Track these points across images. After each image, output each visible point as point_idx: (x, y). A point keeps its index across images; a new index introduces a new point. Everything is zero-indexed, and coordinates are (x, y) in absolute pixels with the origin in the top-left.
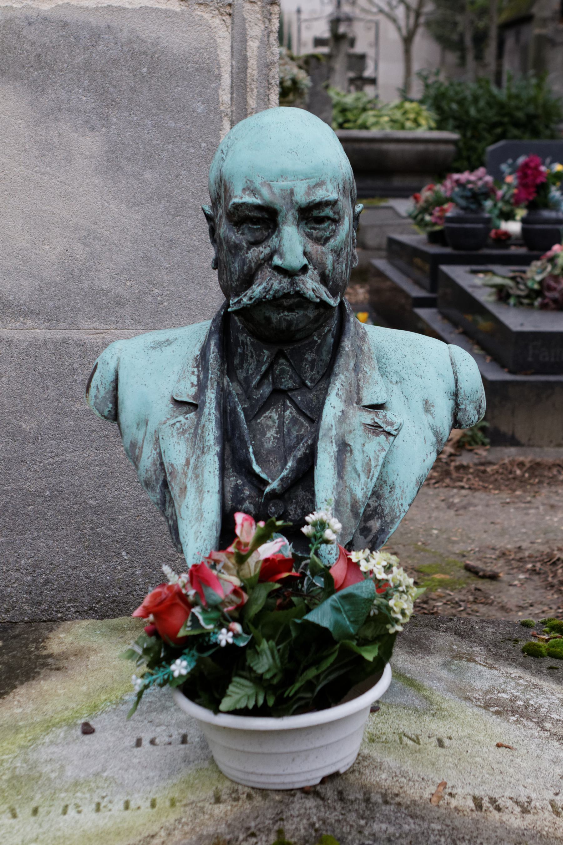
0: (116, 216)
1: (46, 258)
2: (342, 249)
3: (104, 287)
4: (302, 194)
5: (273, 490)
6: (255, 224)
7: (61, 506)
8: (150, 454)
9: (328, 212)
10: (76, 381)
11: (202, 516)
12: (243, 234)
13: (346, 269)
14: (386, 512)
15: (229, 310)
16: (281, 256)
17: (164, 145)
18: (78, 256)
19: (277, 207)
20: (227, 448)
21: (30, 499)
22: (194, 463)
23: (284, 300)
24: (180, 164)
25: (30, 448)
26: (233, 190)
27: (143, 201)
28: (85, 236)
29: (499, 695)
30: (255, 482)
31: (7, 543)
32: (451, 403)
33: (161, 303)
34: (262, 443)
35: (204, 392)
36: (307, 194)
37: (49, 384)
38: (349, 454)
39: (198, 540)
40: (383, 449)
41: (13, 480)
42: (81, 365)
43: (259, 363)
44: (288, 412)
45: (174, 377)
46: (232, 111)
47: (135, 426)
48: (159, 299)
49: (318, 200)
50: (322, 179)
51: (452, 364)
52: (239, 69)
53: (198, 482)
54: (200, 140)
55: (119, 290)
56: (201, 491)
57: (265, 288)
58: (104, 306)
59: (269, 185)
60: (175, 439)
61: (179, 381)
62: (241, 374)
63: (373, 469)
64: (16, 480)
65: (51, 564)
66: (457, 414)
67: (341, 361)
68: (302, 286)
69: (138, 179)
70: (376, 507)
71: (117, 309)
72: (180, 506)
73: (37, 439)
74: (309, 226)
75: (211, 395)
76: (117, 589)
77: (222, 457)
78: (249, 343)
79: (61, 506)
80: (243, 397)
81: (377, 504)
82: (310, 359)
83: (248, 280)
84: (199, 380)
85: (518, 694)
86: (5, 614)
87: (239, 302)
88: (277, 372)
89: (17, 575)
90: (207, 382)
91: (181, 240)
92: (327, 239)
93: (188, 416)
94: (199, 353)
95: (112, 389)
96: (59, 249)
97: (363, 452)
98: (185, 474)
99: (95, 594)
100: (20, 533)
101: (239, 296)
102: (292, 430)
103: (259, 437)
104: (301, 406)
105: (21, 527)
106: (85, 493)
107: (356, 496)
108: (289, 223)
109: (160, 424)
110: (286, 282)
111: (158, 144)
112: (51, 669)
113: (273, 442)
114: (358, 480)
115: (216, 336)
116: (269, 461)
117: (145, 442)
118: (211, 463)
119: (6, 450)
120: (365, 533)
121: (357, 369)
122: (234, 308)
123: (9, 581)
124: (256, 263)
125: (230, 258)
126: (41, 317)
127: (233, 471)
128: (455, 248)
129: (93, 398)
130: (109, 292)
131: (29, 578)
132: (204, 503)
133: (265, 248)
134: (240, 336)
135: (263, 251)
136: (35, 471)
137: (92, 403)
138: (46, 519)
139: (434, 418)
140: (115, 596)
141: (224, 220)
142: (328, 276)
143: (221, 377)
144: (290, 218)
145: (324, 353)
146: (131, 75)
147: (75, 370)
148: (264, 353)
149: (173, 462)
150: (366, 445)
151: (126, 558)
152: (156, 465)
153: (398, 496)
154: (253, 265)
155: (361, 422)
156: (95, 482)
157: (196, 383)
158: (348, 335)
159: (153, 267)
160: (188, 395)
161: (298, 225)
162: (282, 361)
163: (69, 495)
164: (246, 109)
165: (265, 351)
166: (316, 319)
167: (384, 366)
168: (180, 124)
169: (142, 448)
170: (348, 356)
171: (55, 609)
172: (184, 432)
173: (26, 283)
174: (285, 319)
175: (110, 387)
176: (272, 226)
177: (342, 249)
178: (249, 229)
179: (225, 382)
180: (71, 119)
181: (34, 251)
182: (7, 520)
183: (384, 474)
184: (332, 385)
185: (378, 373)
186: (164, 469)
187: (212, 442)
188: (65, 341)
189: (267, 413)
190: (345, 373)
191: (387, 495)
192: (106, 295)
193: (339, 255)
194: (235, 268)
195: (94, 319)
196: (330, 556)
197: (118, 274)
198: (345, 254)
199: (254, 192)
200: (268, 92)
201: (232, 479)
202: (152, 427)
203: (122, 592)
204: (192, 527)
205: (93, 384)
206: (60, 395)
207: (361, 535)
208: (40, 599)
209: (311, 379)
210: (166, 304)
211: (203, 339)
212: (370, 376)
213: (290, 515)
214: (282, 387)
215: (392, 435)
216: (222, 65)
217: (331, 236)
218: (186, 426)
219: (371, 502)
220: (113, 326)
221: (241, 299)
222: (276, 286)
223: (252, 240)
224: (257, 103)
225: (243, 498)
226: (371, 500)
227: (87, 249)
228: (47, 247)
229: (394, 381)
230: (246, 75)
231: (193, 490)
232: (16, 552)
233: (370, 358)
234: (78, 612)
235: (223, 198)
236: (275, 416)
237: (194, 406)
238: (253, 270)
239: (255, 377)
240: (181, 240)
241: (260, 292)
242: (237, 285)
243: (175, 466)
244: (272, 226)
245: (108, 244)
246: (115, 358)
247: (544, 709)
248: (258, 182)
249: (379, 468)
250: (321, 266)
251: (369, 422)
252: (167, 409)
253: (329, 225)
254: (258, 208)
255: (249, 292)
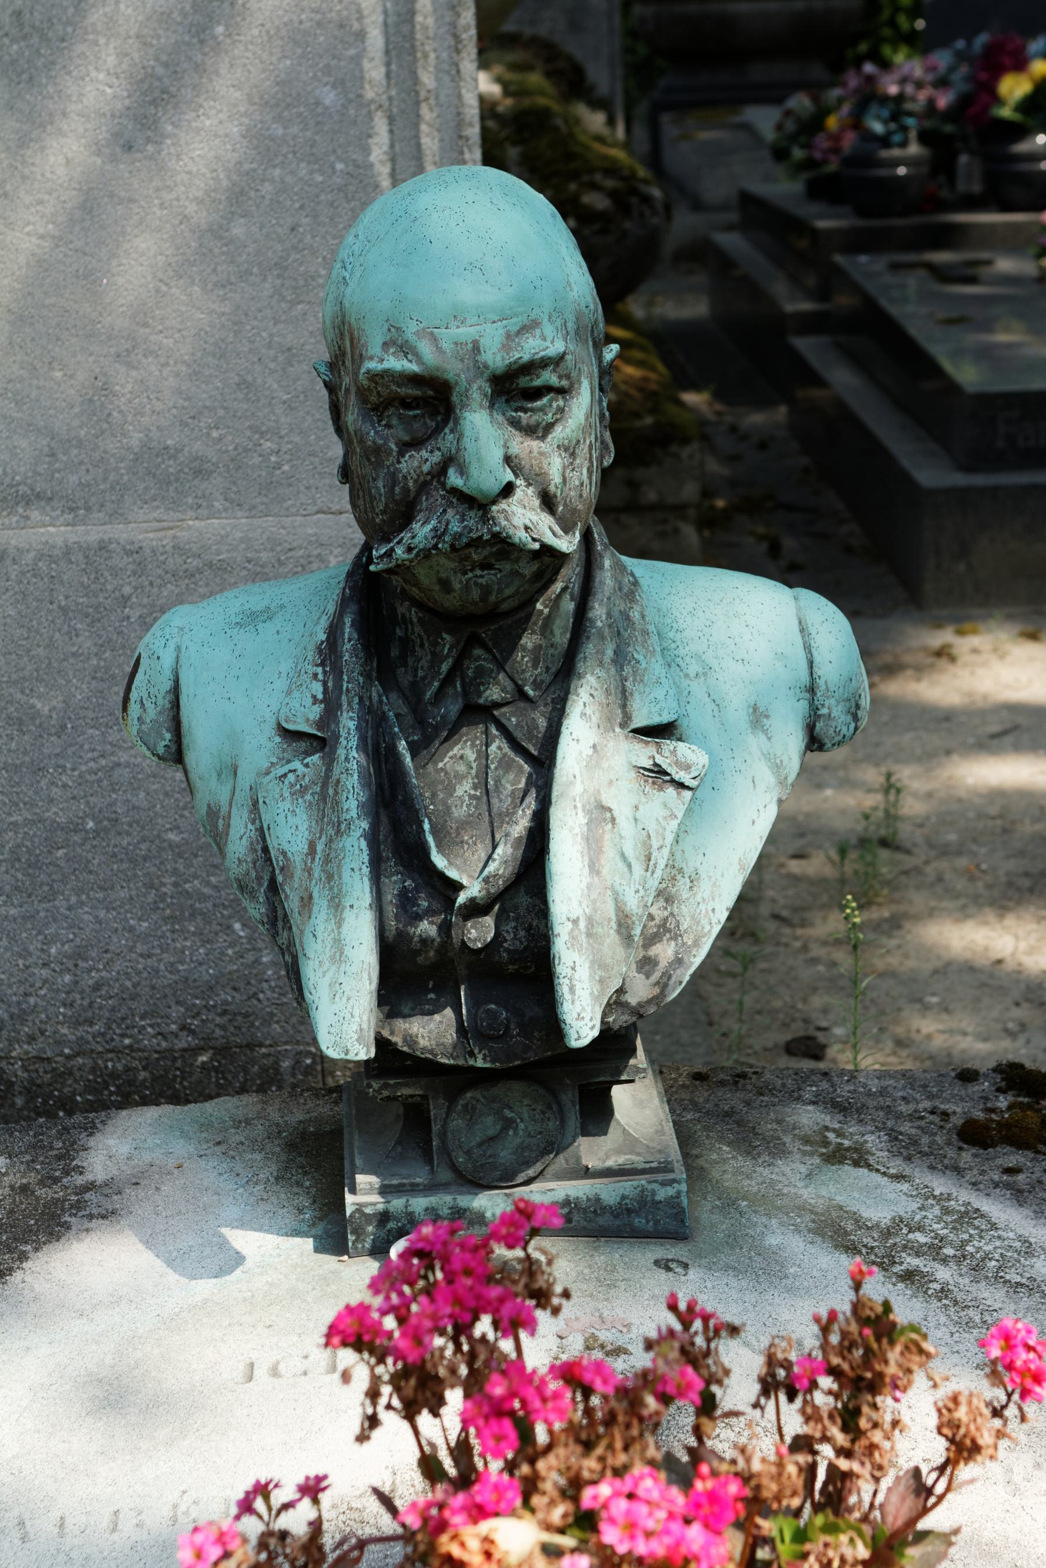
0: (184, 309)
1: (58, 395)
2: (578, 442)
3: (169, 442)
4: (494, 350)
5: (472, 900)
6: (414, 408)
7: (116, 846)
8: (243, 831)
9: (549, 377)
10: (128, 618)
11: (342, 953)
12: (388, 426)
13: (590, 478)
14: (684, 926)
15: (372, 568)
16: (462, 471)
17: (265, 170)
18: (117, 388)
19: (450, 376)
20: (384, 818)
21: (60, 837)
22: (323, 850)
23: (472, 550)
24: (297, 205)
25: (52, 745)
26: (365, 345)
27: (233, 279)
28: (127, 350)
29: (911, 1236)
30: (438, 884)
31: (23, 918)
32: (803, 706)
33: (278, 466)
34: (448, 808)
35: (336, 716)
36: (506, 347)
37: (79, 626)
38: (610, 825)
39: (337, 998)
40: (673, 816)
41: (25, 804)
42: (136, 588)
43: (436, 659)
44: (493, 748)
45: (281, 684)
46: (390, 99)
47: (214, 775)
48: (273, 459)
49: (526, 357)
50: (533, 316)
51: (802, 630)
52: (399, 15)
53: (331, 889)
54: (332, 158)
55: (198, 446)
56: (338, 906)
57: (435, 529)
58: (172, 478)
59: (432, 333)
60: (287, 805)
61: (289, 693)
62: (404, 678)
63: (655, 854)
64: (33, 804)
65: (106, 951)
66: (814, 726)
67: (589, 648)
68: (504, 523)
69: (221, 238)
70: (666, 920)
71: (196, 482)
72: (302, 932)
73: (63, 727)
74: (514, 405)
75: (348, 723)
76: (228, 990)
77: (373, 839)
78: (415, 620)
79: (116, 846)
80: (409, 719)
81: (666, 914)
82: (530, 645)
83: (404, 514)
84: (325, 691)
85: (945, 1231)
86: (29, 1043)
87: (389, 554)
88: (470, 673)
89: (45, 973)
90: (339, 697)
91: (308, 347)
92: (549, 427)
93: (308, 760)
94: (324, 637)
95: (168, 706)
96: (81, 376)
97: (636, 820)
98: (309, 871)
99: (190, 1000)
100: (45, 899)
101: (389, 541)
102: (503, 781)
103: (441, 796)
104: (518, 735)
105: (46, 888)
106: (160, 821)
107: (625, 904)
108: (475, 405)
109: (258, 774)
110: (472, 519)
111: (254, 170)
112: (91, 1217)
113: (468, 806)
114: (628, 875)
115: (354, 607)
116: (462, 842)
117: (234, 806)
118: (355, 851)
119: (9, 751)
120: (647, 968)
121: (621, 659)
122: (380, 567)
123: (32, 986)
124: (416, 481)
125: (368, 470)
126: (55, 503)
127: (396, 864)
128: (863, 212)
129: (136, 722)
130: (178, 451)
131: (67, 978)
132: (345, 928)
133: (432, 452)
134: (397, 605)
135: (418, 462)
136: (65, 786)
137: (134, 731)
138: (91, 872)
139: (769, 739)
140: (226, 1003)
141: (353, 397)
142: (555, 496)
143: (366, 687)
144: (476, 395)
145: (557, 632)
146: (195, 40)
147: (126, 599)
148: (443, 639)
149: (286, 847)
150: (641, 808)
151: (242, 934)
152: (256, 851)
153: (706, 895)
154: (411, 484)
155: (630, 763)
156: (177, 800)
157: (320, 696)
158: (599, 596)
159: (258, 400)
160: (308, 720)
161: (492, 406)
162: (478, 652)
163: (130, 825)
164: (417, 93)
165: (445, 635)
166: (538, 575)
167: (673, 646)
168: (294, 130)
169: (229, 817)
170: (602, 638)
171: (118, 1031)
172: (303, 790)
173: (24, 444)
174: (476, 583)
175: (164, 702)
176: (442, 410)
177: (578, 442)
178: (400, 417)
179: (374, 694)
180: (86, 130)
181: (35, 382)
182: (20, 876)
183: (678, 855)
184: (572, 697)
185: (661, 661)
186: (270, 859)
187: (354, 813)
188: (103, 546)
189: (455, 750)
190: (597, 671)
191: (685, 895)
192: (173, 457)
193: (573, 455)
194: (377, 488)
195: (155, 504)
196: (581, 1023)
197: (194, 418)
198: (586, 449)
199: (405, 349)
200: (456, 58)
201: (394, 878)
202: (246, 777)
203: (237, 995)
204: (324, 973)
205: (134, 696)
206: (102, 646)
207: (639, 972)
208: (90, 1014)
209: (534, 682)
210: (286, 468)
211: (331, 608)
212: (646, 669)
213: (506, 941)
214: (481, 701)
215: (688, 788)
216: (366, 13)
217: (557, 420)
218: (307, 779)
219: (654, 910)
220: (190, 513)
221: (392, 550)
222: (455, 527)
223: (407, 438)
224: (438, 79)
225: (417, 914)
226: (655, 907)
227: (134, 373)
228: (58, 374)
229: (692, 674)
230: (413, 27)
231: (324, 903)
232: (40, 933)
233: (646, 633)
234: (160, 1034)
235: (349, 356)
236: (471, 755)
237: (317, 742)
238: (412, 495)
239: (431, 684)
240: (308, 347)
241: (426, 538)
242: (383, 520)
243: (289, 854)
244: (442, 410)
245: (171, 362)
246: (172, 645)
247: (994, 1263)
248: (411, 329)
249: (666, 851)
250: (539, 479)
251: (648, 764)
252: (270, 745)
253: (551, 401)
254: (415, 379)
255: (406, 536)
